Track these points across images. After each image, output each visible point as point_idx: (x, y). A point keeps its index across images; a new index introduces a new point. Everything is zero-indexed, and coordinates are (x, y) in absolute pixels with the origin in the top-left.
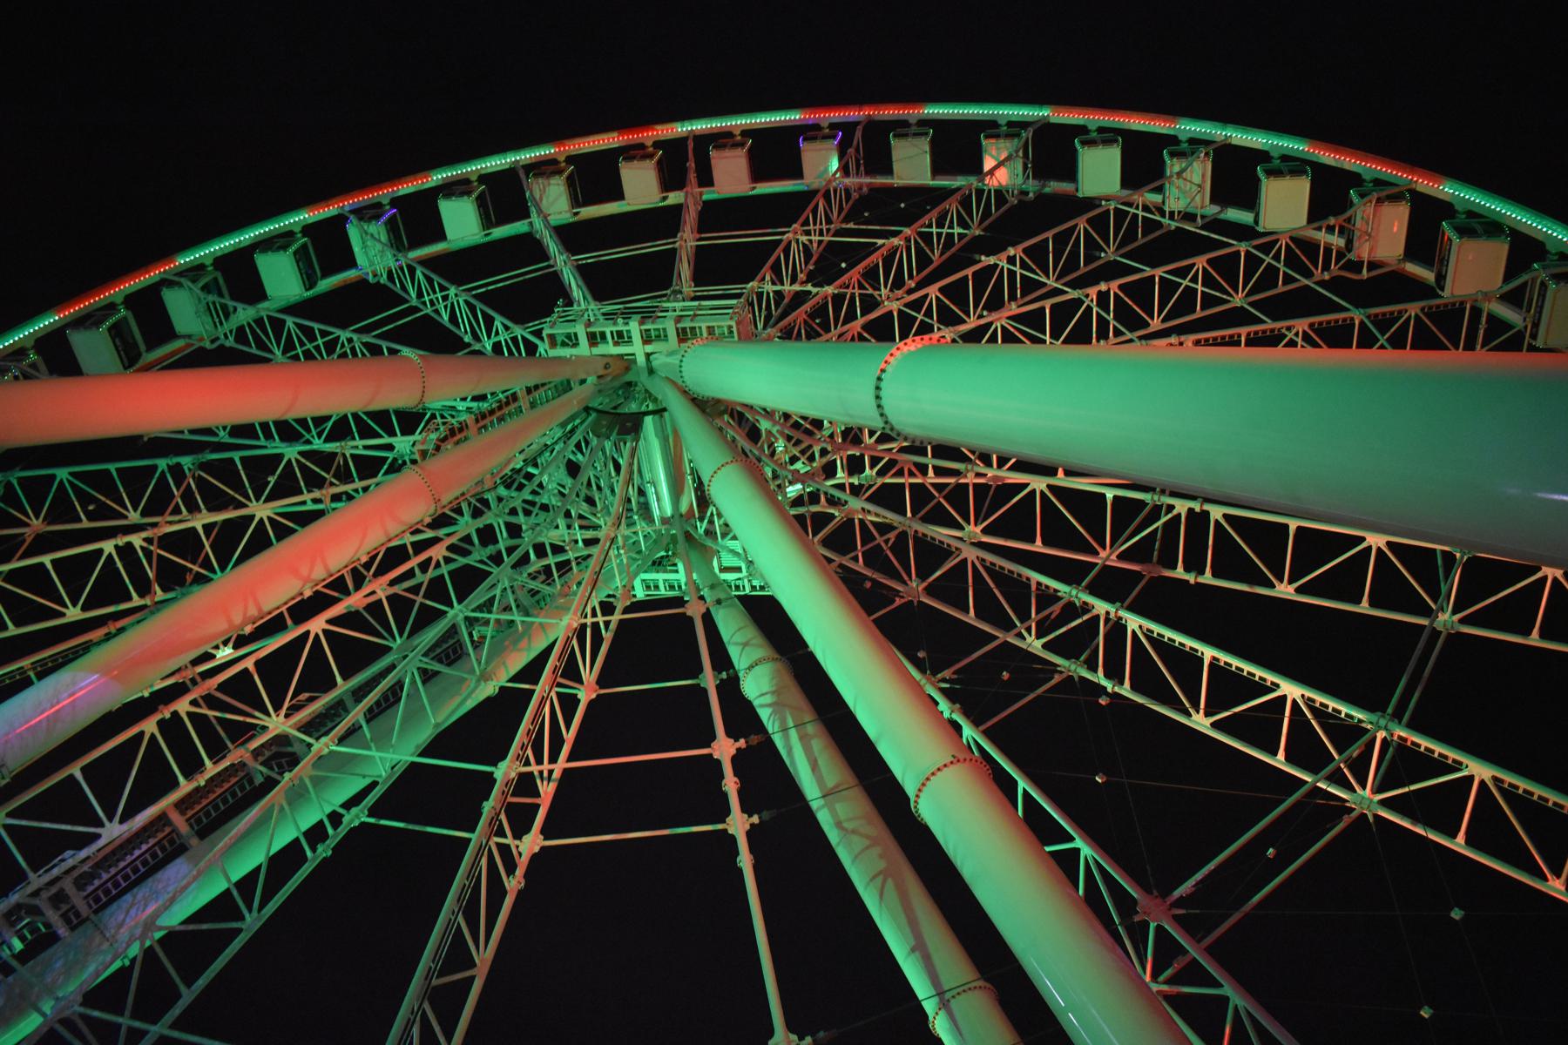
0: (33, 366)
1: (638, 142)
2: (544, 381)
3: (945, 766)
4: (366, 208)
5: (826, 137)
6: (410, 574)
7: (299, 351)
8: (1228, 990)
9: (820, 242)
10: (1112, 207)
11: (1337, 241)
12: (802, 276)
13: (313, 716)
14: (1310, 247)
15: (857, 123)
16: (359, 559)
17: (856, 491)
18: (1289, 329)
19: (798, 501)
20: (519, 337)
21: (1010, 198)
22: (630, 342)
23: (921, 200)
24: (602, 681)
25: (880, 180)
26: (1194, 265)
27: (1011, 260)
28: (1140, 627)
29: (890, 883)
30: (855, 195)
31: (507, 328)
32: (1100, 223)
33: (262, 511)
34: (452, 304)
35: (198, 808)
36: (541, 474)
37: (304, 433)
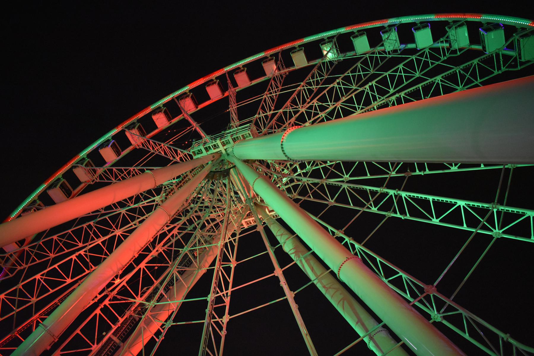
0: (39, 205)
1: (211, 79)
2: (195, 167)
3: (345, 262)
4: (129, 126)
5: (270, 60)
6: (169, 240)
7: (120, 177)
8: (461, 311)
9: (276, 95)
10: (367, 56)
11: (446, 45)
12: (273, 108)
13: (149, 294)
14: (437, 50)
15: (279, 52)
16: (150, 240)
17: (305, 175)
18: (435, 80)
19: (287, 184)
20: (186, 154)
21: (335, 62)
22: (218, 147)
23: (303, 73)
24: (237, 260)
25: (292, 69)
26: (399, 68)
27: (339, 84)
28: (406, 195)
29: (346, 303)
30: (284, 76)
31: (182, 152)
32: (365, 62)
33: (118, 232)
34: (164, 148)
35: (120, 333)
36: (202, 197)
37: (127, 204)
